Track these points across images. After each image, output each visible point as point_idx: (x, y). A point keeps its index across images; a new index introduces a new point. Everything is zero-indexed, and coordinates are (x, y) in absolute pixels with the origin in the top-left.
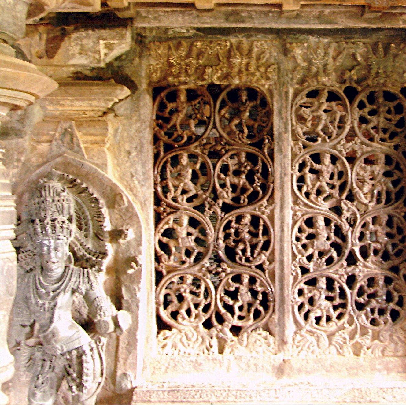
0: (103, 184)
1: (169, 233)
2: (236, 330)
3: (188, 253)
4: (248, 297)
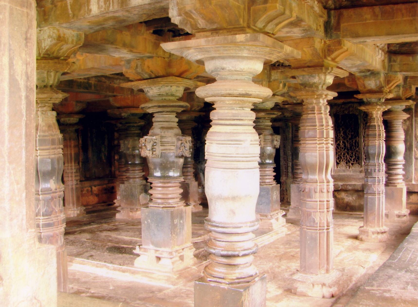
0: (98, 15)
1: (339, 145)
2: (352, 164)
3: (342, 148)
4: (354, 157)
